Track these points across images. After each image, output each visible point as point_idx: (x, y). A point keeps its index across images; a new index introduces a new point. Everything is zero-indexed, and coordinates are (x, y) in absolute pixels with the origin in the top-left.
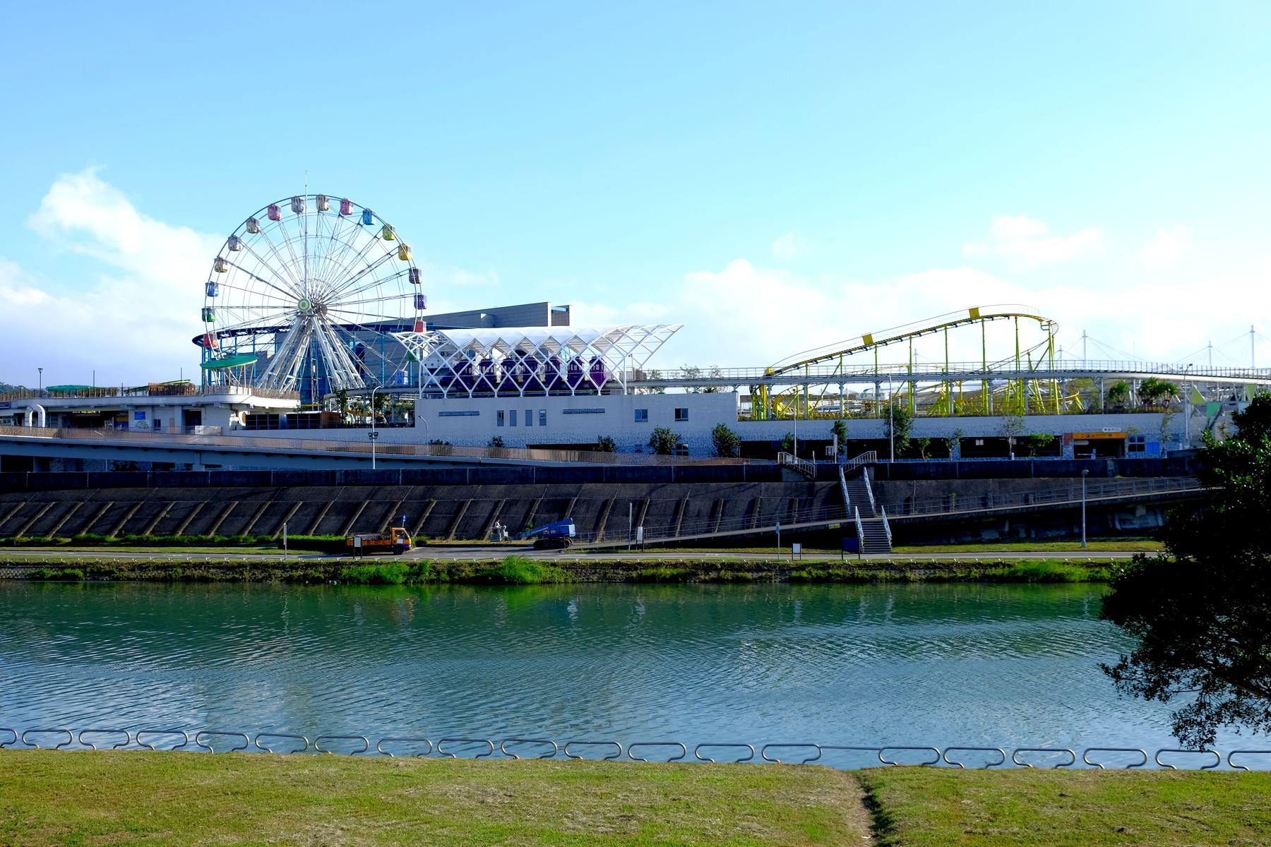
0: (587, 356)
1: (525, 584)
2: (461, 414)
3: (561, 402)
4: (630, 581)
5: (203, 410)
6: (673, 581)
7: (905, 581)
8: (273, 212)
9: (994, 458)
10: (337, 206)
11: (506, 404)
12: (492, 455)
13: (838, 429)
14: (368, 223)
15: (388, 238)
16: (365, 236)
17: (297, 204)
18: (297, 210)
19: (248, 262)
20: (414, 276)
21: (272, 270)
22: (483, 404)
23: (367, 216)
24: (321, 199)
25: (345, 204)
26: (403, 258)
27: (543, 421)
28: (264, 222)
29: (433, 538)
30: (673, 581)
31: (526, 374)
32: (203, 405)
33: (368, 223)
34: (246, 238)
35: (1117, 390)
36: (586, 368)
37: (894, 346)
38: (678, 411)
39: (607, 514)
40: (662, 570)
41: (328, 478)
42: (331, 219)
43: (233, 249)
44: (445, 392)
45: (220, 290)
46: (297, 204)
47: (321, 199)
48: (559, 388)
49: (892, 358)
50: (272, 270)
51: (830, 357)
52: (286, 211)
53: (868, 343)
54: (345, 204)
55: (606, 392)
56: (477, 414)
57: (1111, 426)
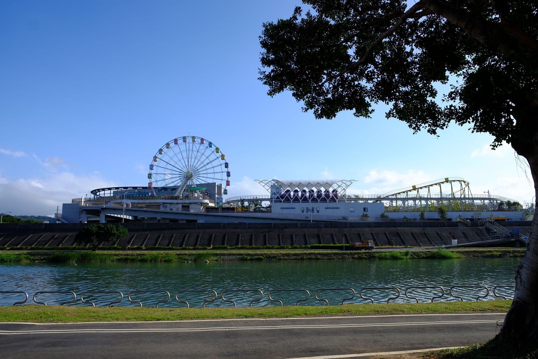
0: (331, 190)
1: (453, 258)
2: (334, 208)
3: (325, 205)
4: (484, 257)
5: (190, 205)
6: (500, 256)
7: (516, 257)
8: (176, 141)
9: (407, 223)
10: (200, 141)
11: (305, 205)
12: (362, 220)
13: (422, 215)
14: (211, 147)
15: (217, 152)
16: (209, 151)
17: (184, 139)
18: (194, 141)
19: (166, 158)
20: (227, 165)
21: (213, 161)
22: (296, 205)
23: (210, 144)
24: (194, 138)
25: (202, 140)
26: (223, 159)
27: (318, 211)
28: (172, 145)
29: (176, 247)
30: (500, 256)
31: (302, 195)
32: (190, 203)
33: (211, 147)
34: (165, 150)
35: (502, 203)
36: (323, 193)
37: (424, 189)
38: (364, 209)
39: (199, 240)
40: (129, 257)
41: (295, 226)
42: (197, 145)
43: (161, 153)
44: (282, 200)
45: (154, 168)
46: (184, 139)
47: (194, 138)
48: (324, 200)
49: (435, 192)
50: (213, 161)
51: (404, 192)
52: (180, 141)
53: (414, 188)
54: (202, 140)
55: (339, 201)
56: (294, 208)
57: (501, 215)
